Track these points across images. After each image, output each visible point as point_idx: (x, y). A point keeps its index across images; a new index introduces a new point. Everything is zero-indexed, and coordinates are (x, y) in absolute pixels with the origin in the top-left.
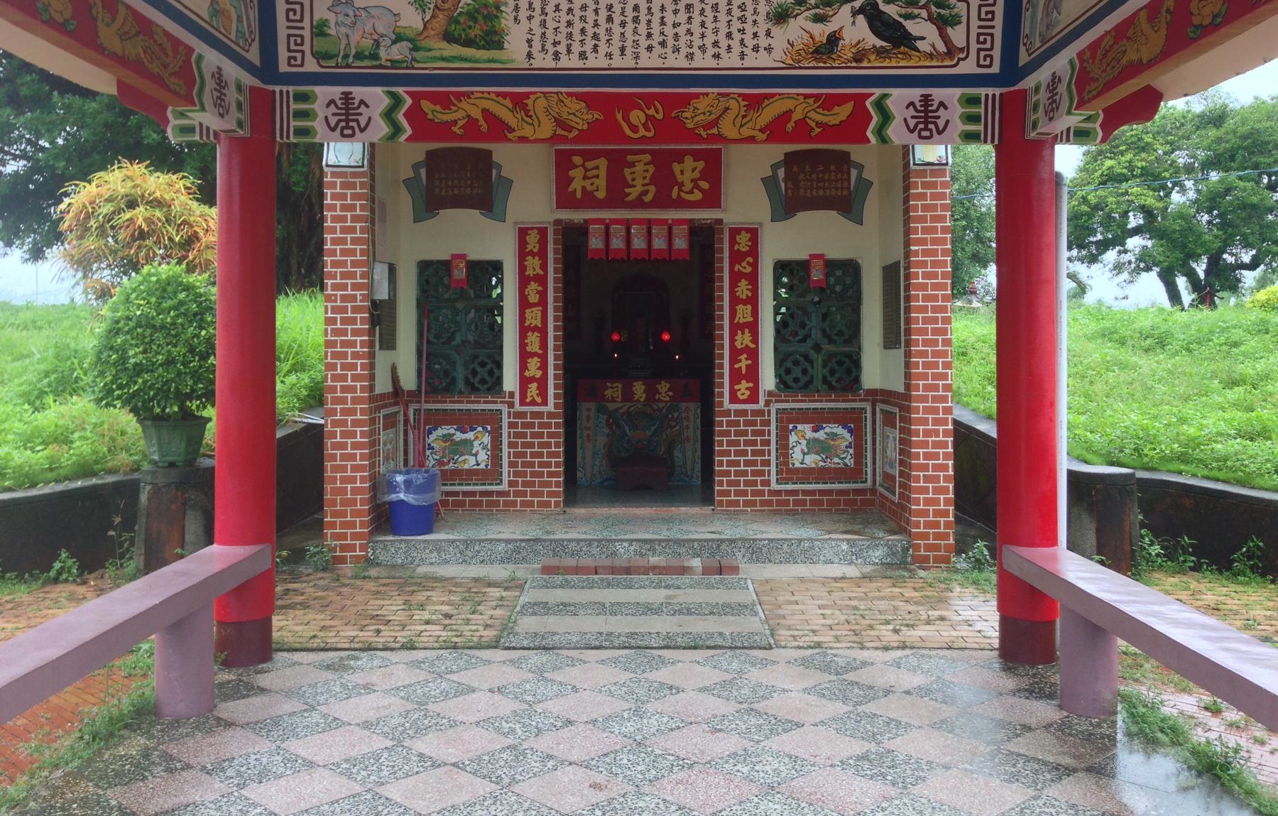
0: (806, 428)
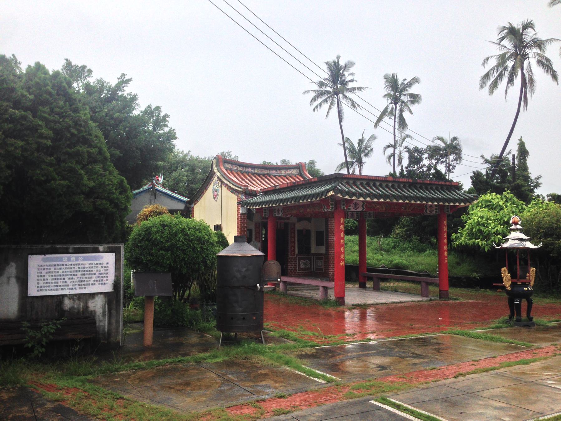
0: (303, 261)
